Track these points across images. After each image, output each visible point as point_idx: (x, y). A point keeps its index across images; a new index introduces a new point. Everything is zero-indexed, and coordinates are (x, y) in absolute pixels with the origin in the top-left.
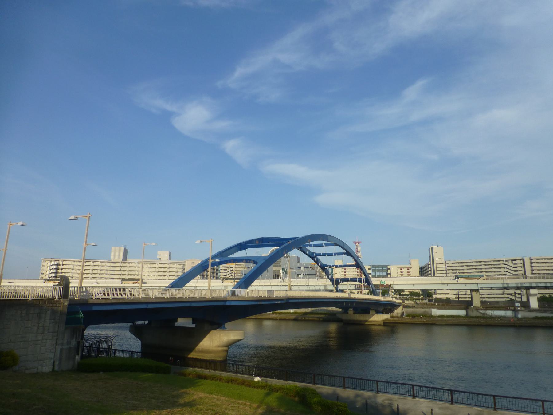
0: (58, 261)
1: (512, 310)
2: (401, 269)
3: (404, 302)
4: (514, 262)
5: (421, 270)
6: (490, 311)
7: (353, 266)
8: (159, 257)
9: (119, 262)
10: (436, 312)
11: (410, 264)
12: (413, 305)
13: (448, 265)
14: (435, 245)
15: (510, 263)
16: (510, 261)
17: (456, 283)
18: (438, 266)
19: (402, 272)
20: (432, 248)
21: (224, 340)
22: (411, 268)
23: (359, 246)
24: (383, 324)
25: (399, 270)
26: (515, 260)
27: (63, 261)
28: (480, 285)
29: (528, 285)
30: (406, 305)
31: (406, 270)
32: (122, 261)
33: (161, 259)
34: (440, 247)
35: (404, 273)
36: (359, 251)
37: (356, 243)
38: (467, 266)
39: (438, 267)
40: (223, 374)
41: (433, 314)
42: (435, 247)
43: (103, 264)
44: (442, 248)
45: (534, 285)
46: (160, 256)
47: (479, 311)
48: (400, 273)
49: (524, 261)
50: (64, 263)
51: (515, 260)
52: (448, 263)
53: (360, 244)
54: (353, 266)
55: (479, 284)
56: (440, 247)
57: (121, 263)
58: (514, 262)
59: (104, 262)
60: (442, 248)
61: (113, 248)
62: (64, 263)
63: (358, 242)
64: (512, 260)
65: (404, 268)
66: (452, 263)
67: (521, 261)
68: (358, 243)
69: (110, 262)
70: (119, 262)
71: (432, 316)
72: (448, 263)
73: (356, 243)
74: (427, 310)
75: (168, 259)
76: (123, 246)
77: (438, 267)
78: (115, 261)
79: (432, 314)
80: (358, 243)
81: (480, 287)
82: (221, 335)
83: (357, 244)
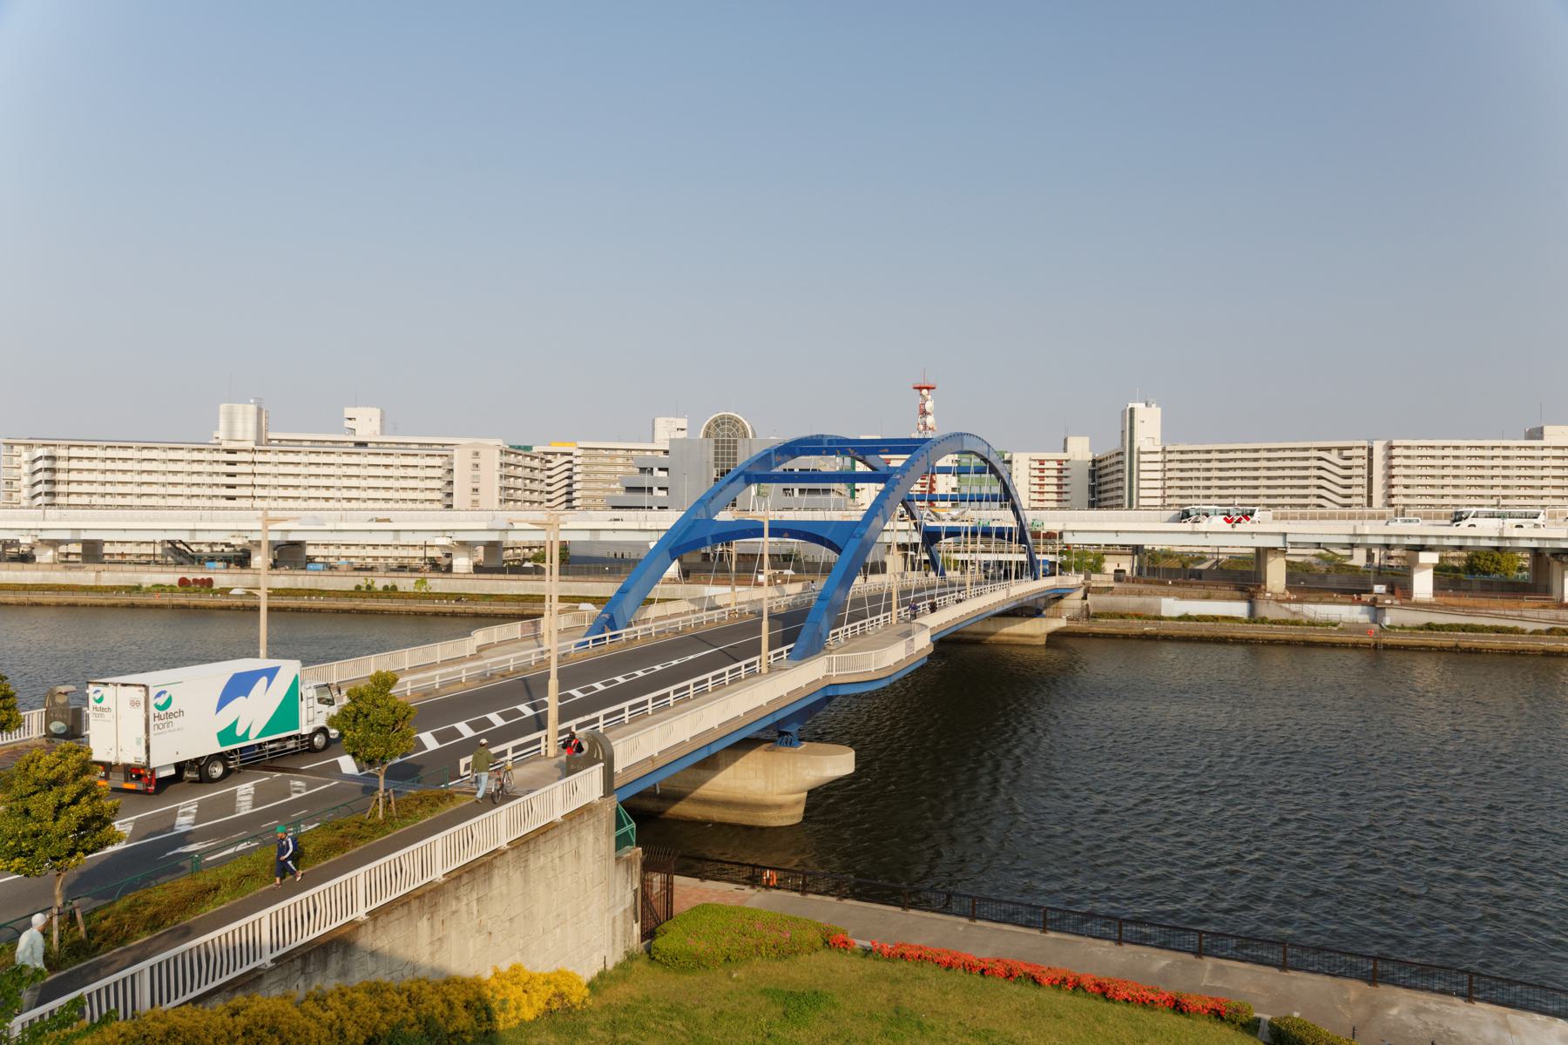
0: (52, 448)
1: (1364, 604)
2: (1042, 462)
3: (1090, 579)
4: (1346, 453)
5: (1094, 465)
6: (1312, 607)
7: (994, 498)
8: (348, 424)
9: (245, 451)
10: (1172, 606)
11: (1065, 450)
12: (1111, 585)
13: (1169, 457)
14: (1140, 402)
15: (1333, 456)
16: (1335, 452)
17: (1231, 530)
18: (1143, 457)
19: (1042, 470)
20: (1132, 410)
21: (808, 778)
22: (1067, 461)
23: (929, 397)
24: (1044, 643)
25: (1036, 465)
26: (1350, 448)
27: (70, 446)
28: (1289, 538)
29: (1417, 541)
30: (1093, 585)
31: (1055, 465)
32: (257, 448)
33: (357, 432)
34: (1154, 405)
35: (1047, 473)
36: (928, 410)
37: (920, 388)
38: (1221, 460)
39: (1144, 462)
40: (927, 918)
41: (1164, 613)
42: (1139, 407)
43: (196, 456)
44: (1159, 409)
45: (1431, 542)
46: (352, 422)
47: (1283, 605)
48: (1037, 473)
49: (1371, 450)
50: (74, 452)
51: (1350, 448)
52: (1170, 452)
53: (931, 391)
54: (994, 498)
55: (1288, 536)
56: (1154, 405)
57: (254, 451)
58: (1346, 453)
59: (200, 450)
60: (1159, 409)
61: (223, 407)
62: (74, 452)
63: (927, 385)
64: (1341, 449)
65: (1048, 460)
66: (1182, 452)
67: (1365, 453)
68: (928, 388)
69: (218, 450)
70: (245, 451)
71: (1160, 618)
72: (1170, 452)
73: (920, 388)
74: (1149, 600)
75: (378, 433)
76: (252, 401)
77: (1144, 462)
78: (233, 446)
79: (1160, 611)
80: (928, 388)
81: (1292, 543)
82: (799, 765)
83: (925, 392)
